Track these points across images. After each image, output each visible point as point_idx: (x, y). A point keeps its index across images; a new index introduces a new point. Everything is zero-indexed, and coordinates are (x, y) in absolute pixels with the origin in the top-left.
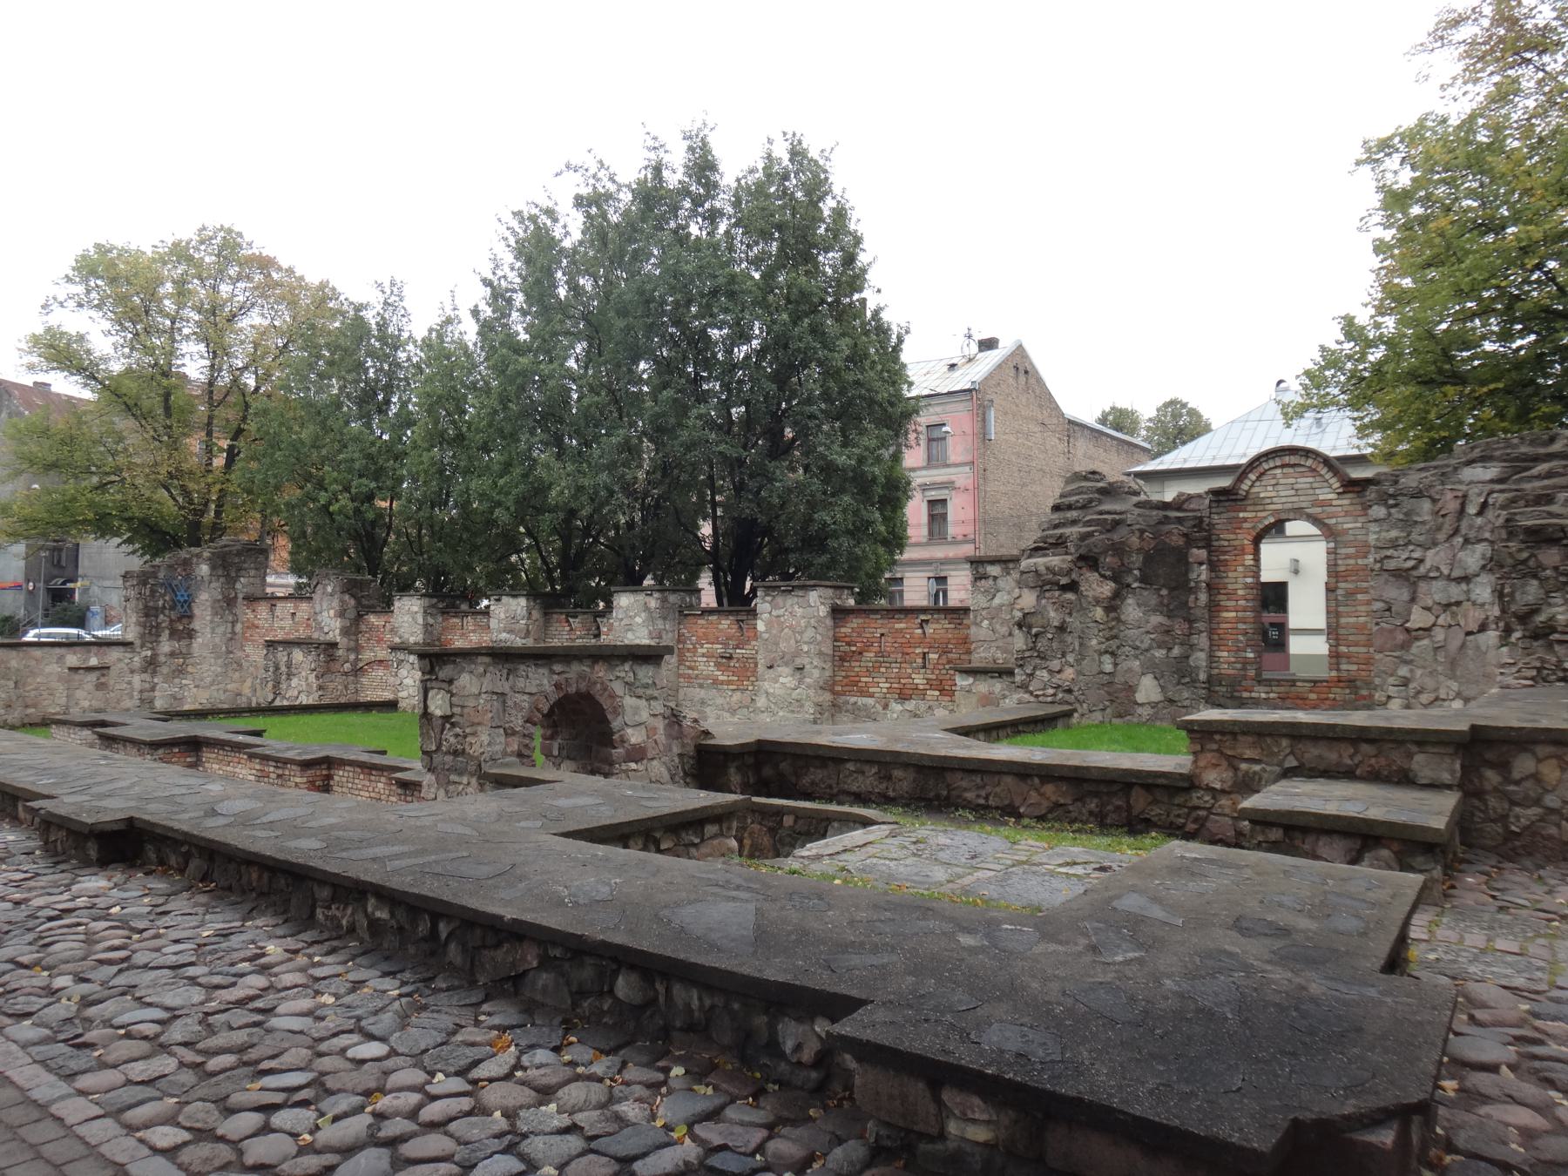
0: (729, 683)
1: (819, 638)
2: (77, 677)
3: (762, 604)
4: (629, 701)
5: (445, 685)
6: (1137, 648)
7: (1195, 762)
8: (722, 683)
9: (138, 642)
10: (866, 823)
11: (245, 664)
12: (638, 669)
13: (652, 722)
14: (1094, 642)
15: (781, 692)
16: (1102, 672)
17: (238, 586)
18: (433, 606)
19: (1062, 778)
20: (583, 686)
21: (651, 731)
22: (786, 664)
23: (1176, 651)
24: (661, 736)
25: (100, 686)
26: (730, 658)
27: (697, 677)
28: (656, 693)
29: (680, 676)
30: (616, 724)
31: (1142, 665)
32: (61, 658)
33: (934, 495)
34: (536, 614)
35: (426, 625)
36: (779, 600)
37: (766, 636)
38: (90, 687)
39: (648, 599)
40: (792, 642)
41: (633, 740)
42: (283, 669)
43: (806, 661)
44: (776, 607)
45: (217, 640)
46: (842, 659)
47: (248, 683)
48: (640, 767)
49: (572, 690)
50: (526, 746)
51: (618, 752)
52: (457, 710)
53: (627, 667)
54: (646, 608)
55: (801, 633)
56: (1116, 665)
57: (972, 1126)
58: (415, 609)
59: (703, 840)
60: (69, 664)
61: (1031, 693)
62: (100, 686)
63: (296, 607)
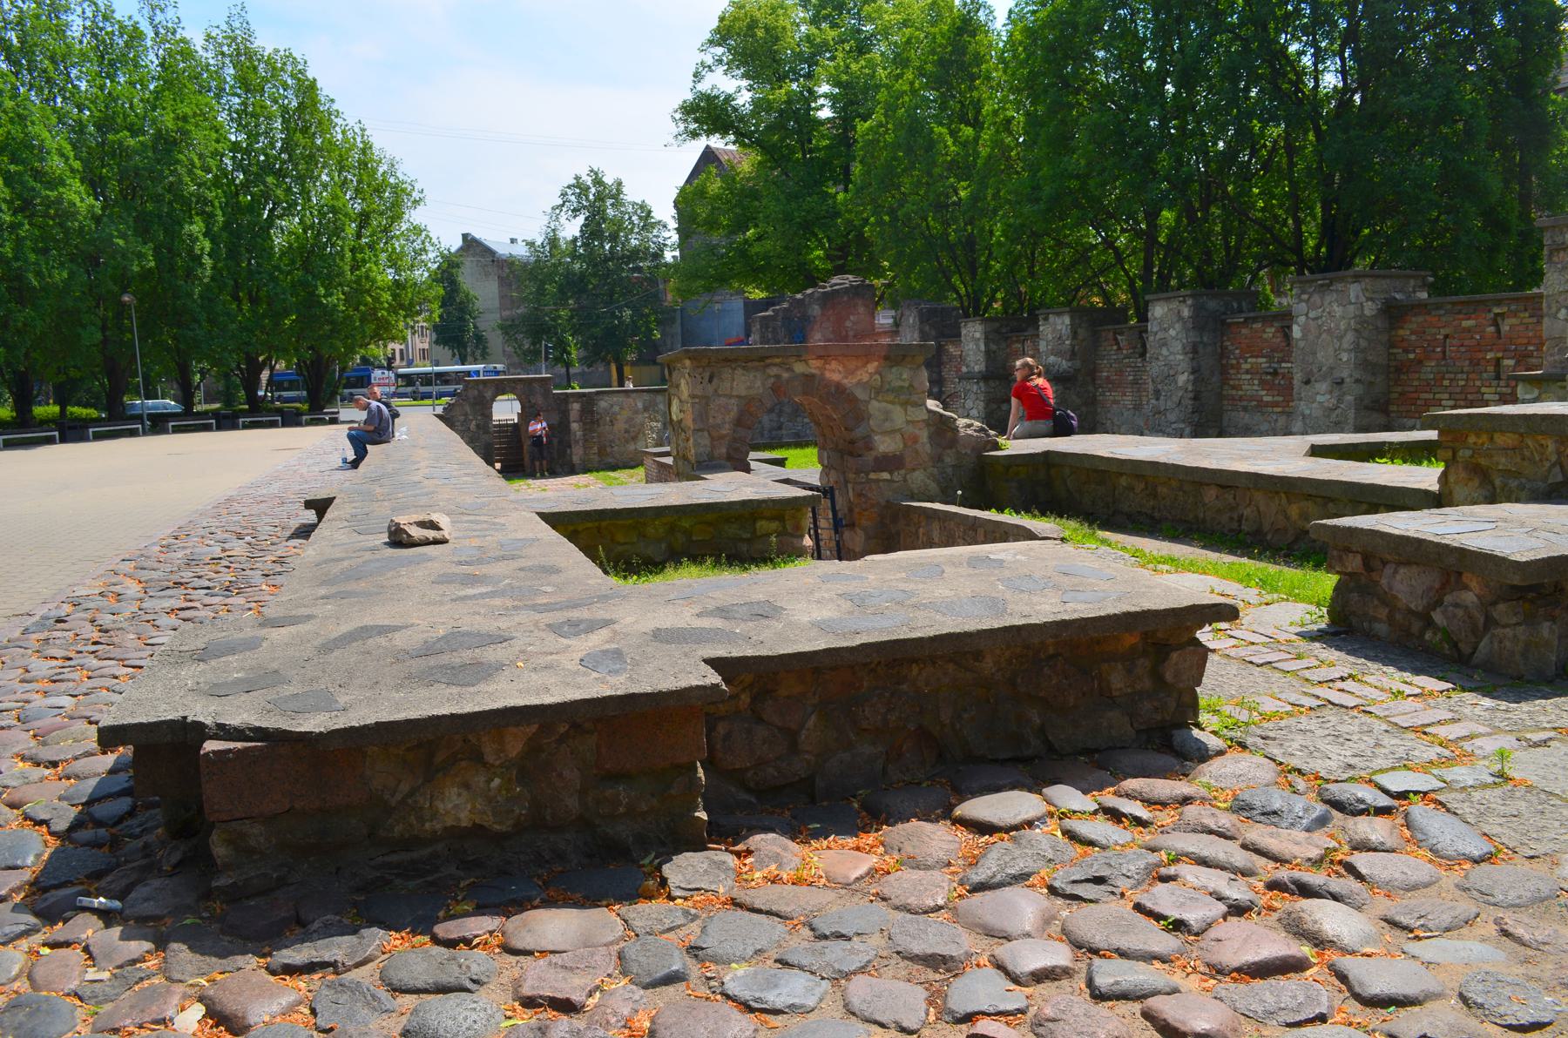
0: (1276, 404)
4: (875, 406)
8: (1267, 404)
10: (1030, 535)
13: (910, 429)
17: (848, 324)
18: (997, 331)
22: (1324, 378)
27: (1241, 398)
34: (1082, 333)
35: (988, 352)
36: (1316, 298)
37: (1301, 344)
40: (1331, 350)
43: (1345, 374)
44: (1311, 307)
46: (1398, 370)
48: (897, 476)
50: (736, 450)
54: (1180, 318)
55: (1340, 338)
57: (441, 914)
58: (978, 335)
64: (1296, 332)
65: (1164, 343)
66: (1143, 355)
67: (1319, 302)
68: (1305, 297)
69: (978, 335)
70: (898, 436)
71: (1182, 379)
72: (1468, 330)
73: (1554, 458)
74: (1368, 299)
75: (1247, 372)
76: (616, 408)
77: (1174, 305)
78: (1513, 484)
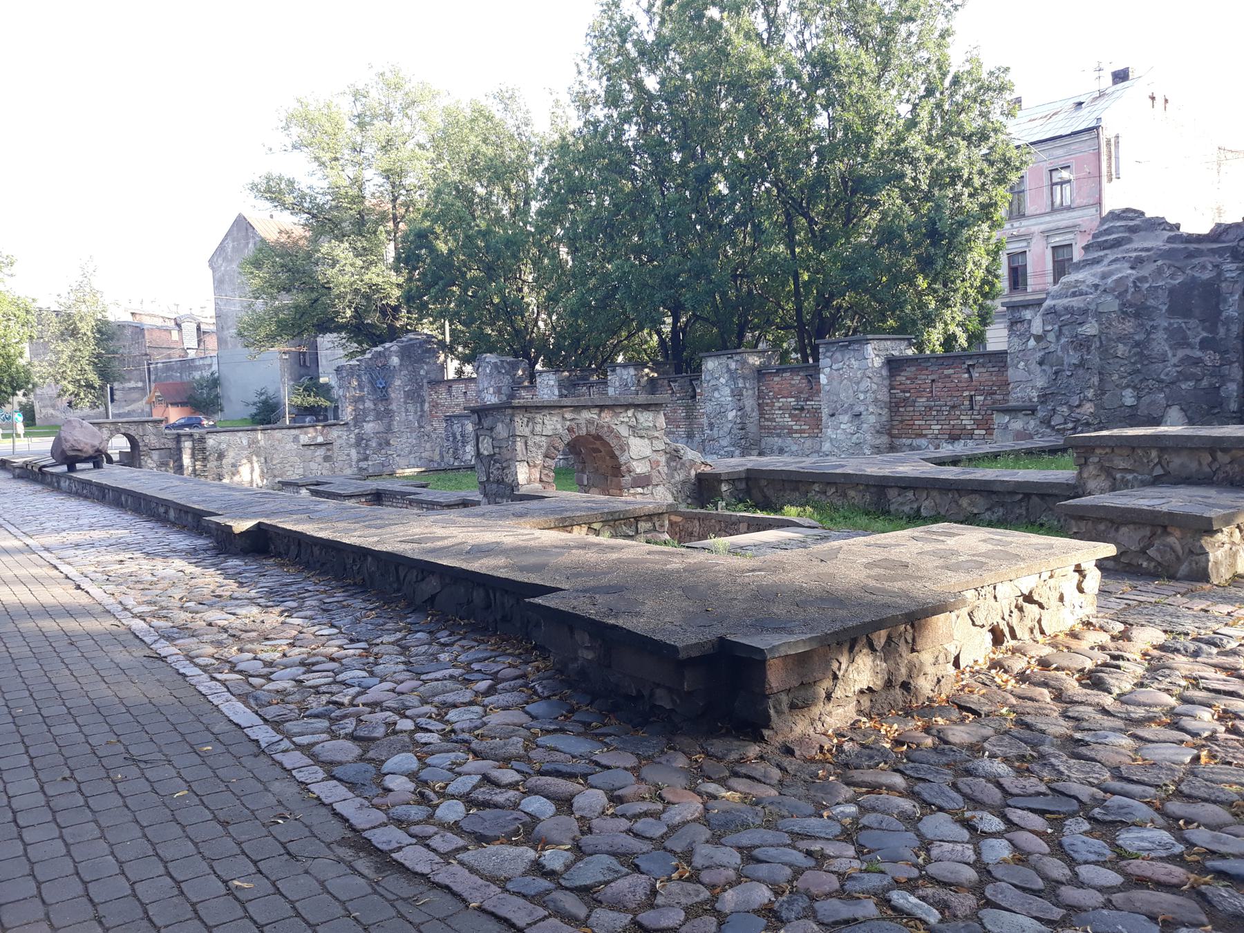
0: (801, 431)
1: (874, 387)
2: (309, 452)
3: (824, 362)
5: (488, 432)
6: (1161, 381)
7: (1080, 473)
9: (352, 423)
11: (434, 436)
12: (639, 415)
14: (1115, 377)
15: (842, 437)
16: (1123, 405)
19: (974, 491)
20: (593, 430)
21: (654, 464)
23: (1205, 383)
24: (664, 469)
25: (327, 459)
26: (802, 409)
28: (656, 434)
29: (761, 427)
30: (622, 460)
31: (1167, 398)
32: (296, 439)
33: (1057, 240)
36: (838, 355)
37: (827, 388)
38: (319, 459)
39: (730, 361)
40: (851, 391)
41: (638, 471)
42: (459, 437)
45: (411, 418)
47: (437, 451)
49: (584, 432)
51: (628, 478)
52: (497, 450)
53: (630, 413)
55: (858, 383)
56: (1139, 398)
58: (552, 383)
59: (637, 532)
60: (302, 442)
61: (1053, 428)
62: (327, 459)
63: (466, 387)
64: (823, 379)
65: (716, 389)
66: (694, 397)
67: (840, 358)
68: (829, 354)
69: (552, 383)
70: (648, 464)
71: (731, 415)
72: (949, 376)
73: (1156, 461)
74: (877, 355)
75: (780, 409)
76: (224, 446)
77: (724, 360)
78: (1130, 477)
